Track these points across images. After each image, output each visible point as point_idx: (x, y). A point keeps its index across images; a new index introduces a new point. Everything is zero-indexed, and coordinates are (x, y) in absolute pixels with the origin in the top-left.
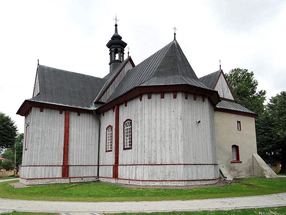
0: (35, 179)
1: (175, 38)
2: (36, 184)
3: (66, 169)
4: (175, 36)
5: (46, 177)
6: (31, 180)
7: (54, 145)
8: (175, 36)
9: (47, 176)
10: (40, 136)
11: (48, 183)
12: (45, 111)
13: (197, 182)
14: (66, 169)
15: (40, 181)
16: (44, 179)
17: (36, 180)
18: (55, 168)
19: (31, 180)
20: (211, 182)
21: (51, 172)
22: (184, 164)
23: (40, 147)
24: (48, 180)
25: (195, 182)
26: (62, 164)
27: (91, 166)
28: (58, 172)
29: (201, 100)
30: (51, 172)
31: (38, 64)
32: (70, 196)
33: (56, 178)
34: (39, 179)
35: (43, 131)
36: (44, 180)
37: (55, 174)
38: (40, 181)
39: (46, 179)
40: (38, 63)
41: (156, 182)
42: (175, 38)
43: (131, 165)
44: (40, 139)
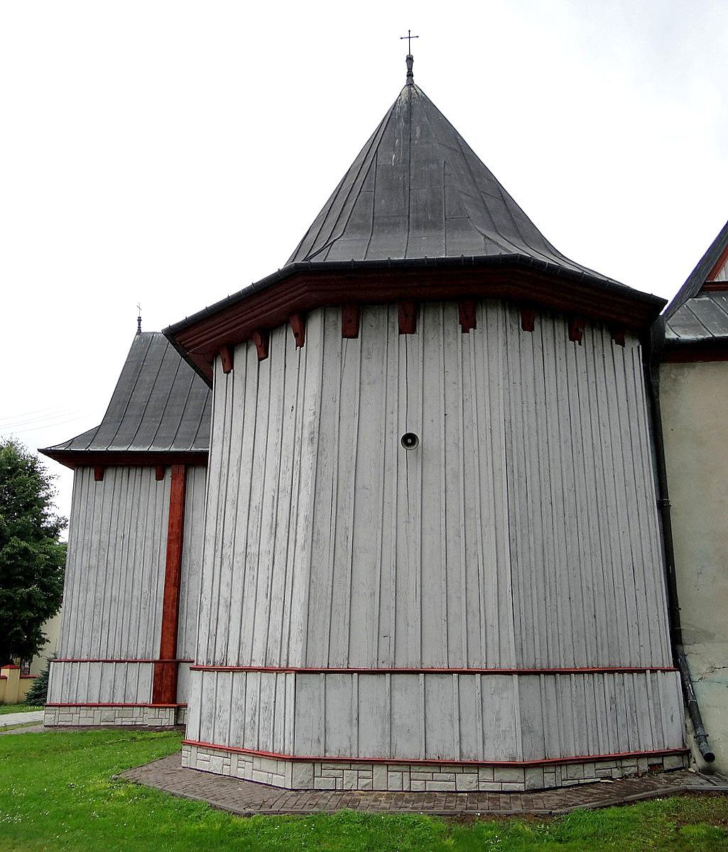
0: (70, 706)
1: (410, 75)
2: (70, 724)
3: (166, 675)
4: (410, 69)
5: (105, 701)
6: (87, 708)
7: (135, 590)
8: (410, 69)
9: (107, 696)
10: (94, 562)
11: (107, 721)
12: (109, 475)
13: (380, 771)
14: (166, 675)
15: (83, 712)
16: (98, 706)
17: (73, 709)
18: (133, 668)
19: (57, 708)
20: (488, 782)
21: (120, 683)
22: (520, 673)
23: (91, 596)
24: (108, 713)
25: (368, 774)
26: (157, 657)
27: (86, 662)
28: (142, 684)
29: (453, 325)
30: (120, 683)
31: (139, 332)
32: (48, 778)
33: (133, 706)
34: (80, 706)
35: (103, 545)
36: (97, 711)
37: (133, 690)
38: (85, 715)
39: (105, 708)
40: (139, 327)
41: (216, 753)
42: (410, 75)
43: (121, 661)
44: (93, 572)
